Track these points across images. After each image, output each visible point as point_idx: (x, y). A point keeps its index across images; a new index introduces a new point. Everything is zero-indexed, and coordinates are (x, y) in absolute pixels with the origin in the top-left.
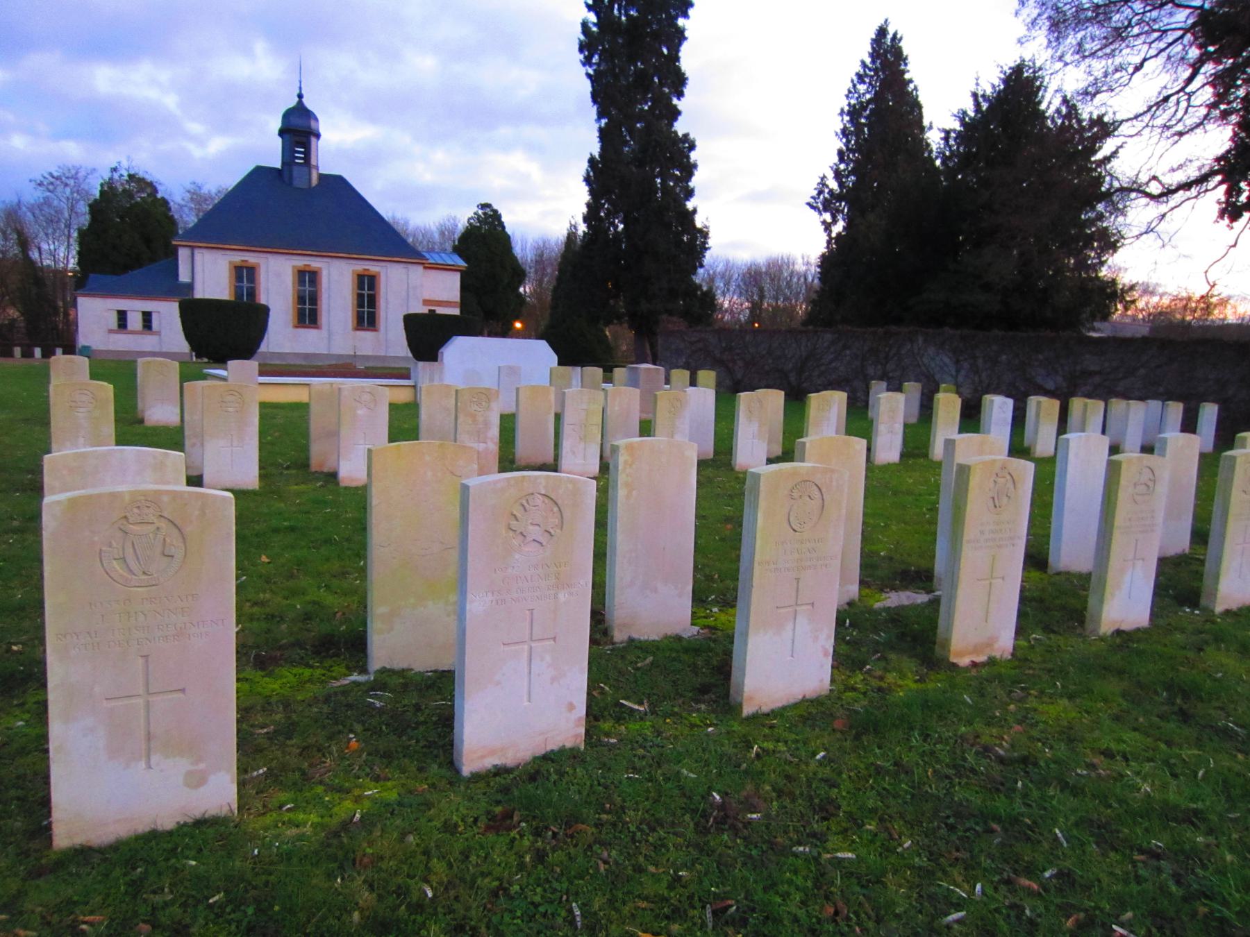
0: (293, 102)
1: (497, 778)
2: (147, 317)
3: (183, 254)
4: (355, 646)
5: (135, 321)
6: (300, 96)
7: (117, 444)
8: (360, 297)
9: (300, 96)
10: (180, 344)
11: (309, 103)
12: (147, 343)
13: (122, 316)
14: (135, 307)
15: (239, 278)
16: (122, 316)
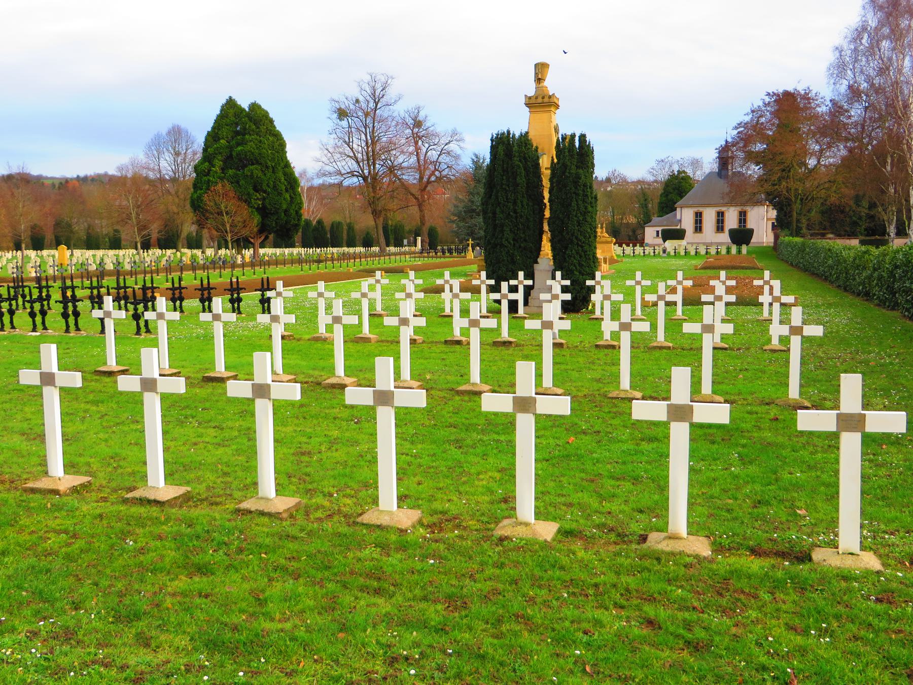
3: (678, 210)
16: (658, 232)
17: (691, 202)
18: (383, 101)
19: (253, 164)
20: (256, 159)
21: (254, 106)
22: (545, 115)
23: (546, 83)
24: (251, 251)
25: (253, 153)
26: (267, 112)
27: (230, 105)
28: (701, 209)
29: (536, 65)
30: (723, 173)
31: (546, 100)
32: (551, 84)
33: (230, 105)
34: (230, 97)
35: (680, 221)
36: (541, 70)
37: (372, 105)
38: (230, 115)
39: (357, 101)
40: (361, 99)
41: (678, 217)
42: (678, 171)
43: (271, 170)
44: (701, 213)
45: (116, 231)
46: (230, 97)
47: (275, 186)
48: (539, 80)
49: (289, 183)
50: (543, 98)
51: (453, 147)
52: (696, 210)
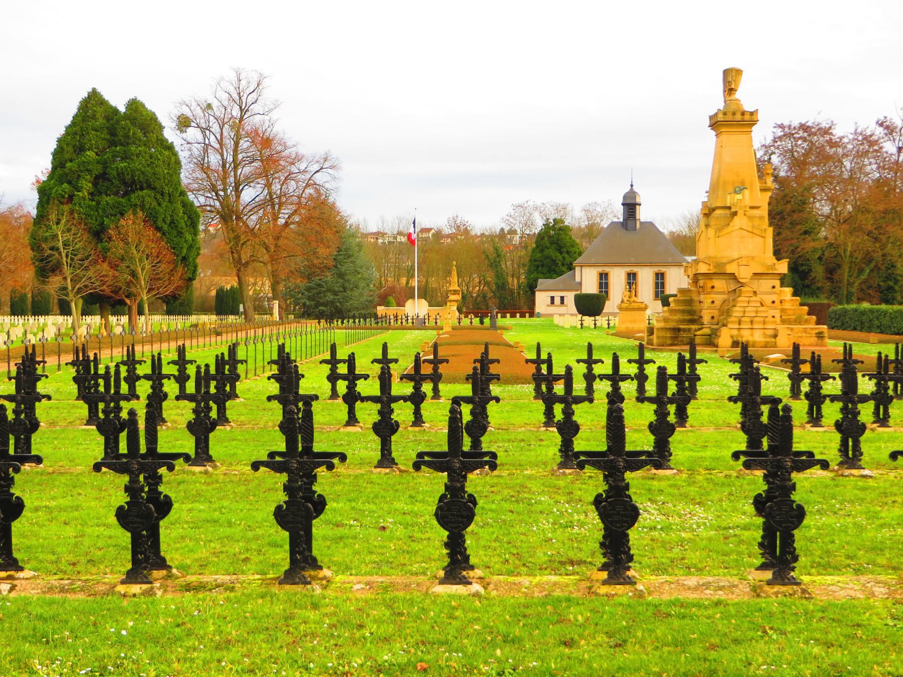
0: (628, 189)
1: (721, 592)
2: (562, 298)
3: (578, 270)
4: (785, 274)
5: (557, 301)
6: (632, 186)
7: (817, 324)
8: (657, 284)
9: (632, 186)
10: (574, 310)
11: (635, 189)
12: (562, 310)
13: (552, 298)
14: (557, 295)
15: (601, 278)
16: (552, 298)
17: (593, 260)
18: (255, 108)
19: (142, 189)
20: (147, 181)
21: (134, 105)
22: (744, 137)
23: (738, 95)
24: (125, 319)
25: (143, 173)
26: (154, 114)
27: (93, 104)
28: (607, 270)
29: (726, 73)
30: (630, 223)
31: (747, 117)
32: (747, 97)
33: (93, 104)
34: (94, 90)
35: (581, 283)
36: (731, 79)
37: (236, 112)
38: (98, 115)
39: (209, 106)
40: (215, 104)
41: (578, 279)
42: (555, 220)
43: (167, 198)
44: (607, 275)
45: (44, 282)
46: (94, 90)
47: (172, 222)
48: (729, 90)
49: (189, 218)
50: (734, 114)
51: (319, 178)
52: (600, 270)
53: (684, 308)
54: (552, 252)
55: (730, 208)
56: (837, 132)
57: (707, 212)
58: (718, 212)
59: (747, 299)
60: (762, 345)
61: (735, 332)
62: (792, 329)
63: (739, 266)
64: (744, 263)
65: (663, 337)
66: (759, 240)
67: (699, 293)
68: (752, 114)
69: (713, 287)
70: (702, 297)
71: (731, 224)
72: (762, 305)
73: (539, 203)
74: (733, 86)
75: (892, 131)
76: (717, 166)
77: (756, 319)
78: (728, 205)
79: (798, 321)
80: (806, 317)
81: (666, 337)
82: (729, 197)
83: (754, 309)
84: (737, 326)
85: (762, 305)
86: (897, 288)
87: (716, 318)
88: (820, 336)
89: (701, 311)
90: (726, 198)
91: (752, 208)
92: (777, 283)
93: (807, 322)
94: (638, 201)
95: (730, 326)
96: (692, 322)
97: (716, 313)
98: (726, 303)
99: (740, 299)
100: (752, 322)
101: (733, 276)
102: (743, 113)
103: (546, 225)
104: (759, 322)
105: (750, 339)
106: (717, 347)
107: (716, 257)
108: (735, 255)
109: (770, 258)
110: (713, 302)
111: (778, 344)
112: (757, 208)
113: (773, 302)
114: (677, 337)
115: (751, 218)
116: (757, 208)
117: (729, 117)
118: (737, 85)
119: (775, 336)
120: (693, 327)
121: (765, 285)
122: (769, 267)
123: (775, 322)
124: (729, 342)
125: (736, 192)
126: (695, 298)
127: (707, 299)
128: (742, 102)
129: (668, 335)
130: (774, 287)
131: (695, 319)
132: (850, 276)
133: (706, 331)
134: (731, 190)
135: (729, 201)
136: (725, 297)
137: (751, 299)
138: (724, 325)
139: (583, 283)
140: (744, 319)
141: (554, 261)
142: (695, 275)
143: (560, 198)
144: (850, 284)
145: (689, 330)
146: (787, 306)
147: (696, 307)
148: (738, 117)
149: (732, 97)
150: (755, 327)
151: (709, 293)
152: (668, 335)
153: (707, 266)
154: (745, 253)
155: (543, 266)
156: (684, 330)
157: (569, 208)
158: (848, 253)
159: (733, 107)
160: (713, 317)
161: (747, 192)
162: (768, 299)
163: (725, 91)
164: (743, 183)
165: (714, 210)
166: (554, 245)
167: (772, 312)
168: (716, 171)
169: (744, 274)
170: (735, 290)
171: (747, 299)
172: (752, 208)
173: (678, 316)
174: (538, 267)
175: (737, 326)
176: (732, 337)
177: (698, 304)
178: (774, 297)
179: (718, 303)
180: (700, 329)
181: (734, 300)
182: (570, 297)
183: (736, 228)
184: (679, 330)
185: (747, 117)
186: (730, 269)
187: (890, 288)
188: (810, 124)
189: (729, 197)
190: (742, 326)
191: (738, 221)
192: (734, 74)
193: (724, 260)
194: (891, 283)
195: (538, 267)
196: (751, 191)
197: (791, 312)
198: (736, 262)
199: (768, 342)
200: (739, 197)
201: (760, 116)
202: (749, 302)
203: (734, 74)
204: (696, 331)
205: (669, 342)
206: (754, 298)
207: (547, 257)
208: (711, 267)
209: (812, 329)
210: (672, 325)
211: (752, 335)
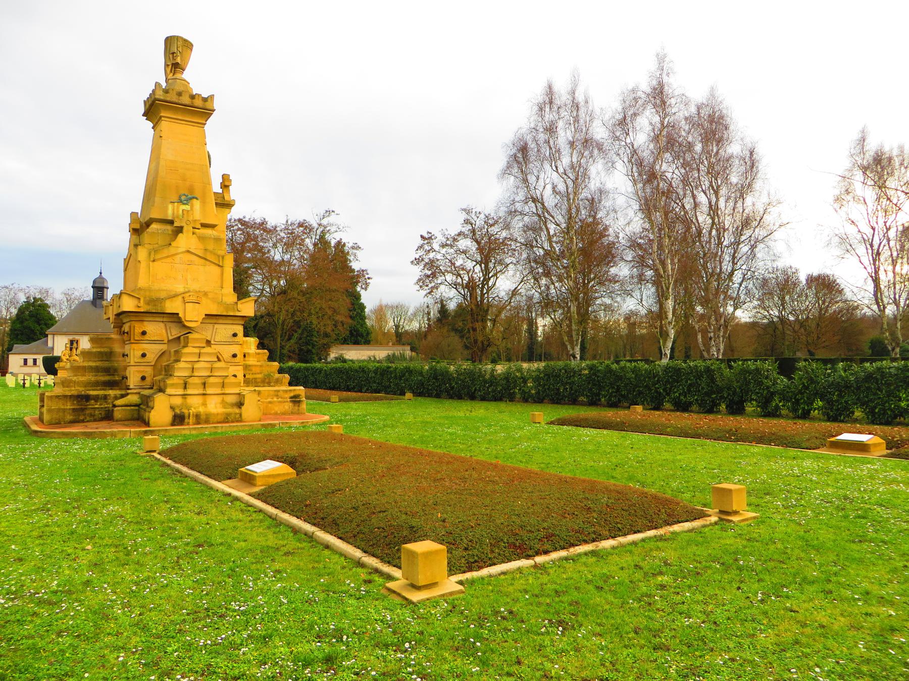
2: (35, 361)
3: (50, 337)
5: (30, 362)
13: (25, 361)
14: (30, 358)
16: (25, 361)
17: (65, 330)
23: (187, 75)
35: (53, 348)
36: (176, 52)
41: (50, 344)
48: (174, 66)
50: (180, 94)
53: (98, 364)
54: (31, 323)
55: (171, 222)
56: (271, 223)
57: (137, 226)
58: (154, 226)
59: (197, 351)
60: (220, 418)
61: (177, 401)
62: (259, 393)
63: (185, 303)
64: (194, 299)
65: (59, 410)
66: (217, 270)
67: (124, 342)
68: (205, 100)
69: (144, 333)
70: (127, 349)
71: (173, 244)
72: (219, 360)
73: (23, 286)
74: (179, 60)
75: (310, 230)
76: (154, 164)
77: (211, 380)
78: (170, 218)
79: (267, 381)
80: (277, 375)
81: (64, 410)
82: (170, 207)
83: (208, 365)
84: (181, 392)
85: (219, 360)
86: (314, 351)
87: (148, 380)
88: (296, 400)
89: (125, 368)
90: (166, 209)
91: (204, 226)
92: (240, 330)
93: (278, 382)
94: (105, 285)
95: (169, 391)
96: (111, 385)
97: (148, 372)
98: (165, 358)
99: (186, 350)
100: (204, 384)
101: (175, 318)
102: (193, 97)
103: (27, 303)
104: (214, 385)
105: (201, 410)
106: (147, 424)
107: (150, 290)
108: (180, 288)
109: (230, 296)
110: (144, 355)
111: (244, 416)
112: (213, 226)
113: (234, 356)
114: (83, 410)
115: (202, 238)
116: (213, 226)
117: (172, 97)
118: (186, 60)
119: (240, 405)
120: (112, 393)
121: (224, 331)
122: (227, 306)
123: (238, 385)
124: (168, 416)
125: (181, 201)
126: (117, 349)
127: (134, 352)
128: (191, 86)
129: (69, 406)
130: (235, 335)
131: (113, 378)
132: (282, 340)
133: (133, 398)
134: (175, 198)
135: (170, 212)
136: (164, 347)
137: (203, 351)
138: (161, 390)
139: (55, 348)
140: (191, 380)
141: (32, 331)
142: (118, 315)
143: (43, 283)
144: (282, 347)
145: (105, 397)
146: (251, 361)
147: (119, 363)
148: (186, 100)
149: (178, 76)
150: (209, 391)
151: (138, 342)
152: (69, 406)
153: (135, 302)
154: (194, 286)
155: (22, 334)
156: (96, 398)
157: (50, 291)
158: (280, 322)
159: (178, 87)
160: (143, 378)
161: (197, 204)
162: (227, 351)
163: (166, 65)
164: (191, 189)
165: (148, 224)
166: (33, 319)
167: (233, 370)
168: (151, 178)
169: (192, 315)
170: (179, 338)
171: (197, 351)
172: (204, 226)
173: (90, 377)
174: (17, 335)
175: (181, 392)
176: (172, 408)
177: (121, 359)
178: (235, 349)
179: (151, 358)
180: (123, 396)
181: (177, 352)
182: (40, 358)
183: (181, 250)
184: (87, 398)
185: (198, 103)
186: (171, 307)
187: (309, 351)
188: (247, 219)
189: (170, 207)
190: (189, 392)
191: (184, 241)
192: (180, 43)
193: (163, 295)
194: (310, 348)
195: (17, 335)
196: (204, 203)
197: (258, 370)
198: (180, 297)
199: (228, 414)
200: (187, 207)
201: (216, 105)
202: (199, 355)
203: (180, 43)
204: (116, 398)
205: (69, 417)
206: (208, 350)
207: (26, 328)
208: (142, 303)
209: (286, 391)
210: (73, 391)
211: (204, 404)
